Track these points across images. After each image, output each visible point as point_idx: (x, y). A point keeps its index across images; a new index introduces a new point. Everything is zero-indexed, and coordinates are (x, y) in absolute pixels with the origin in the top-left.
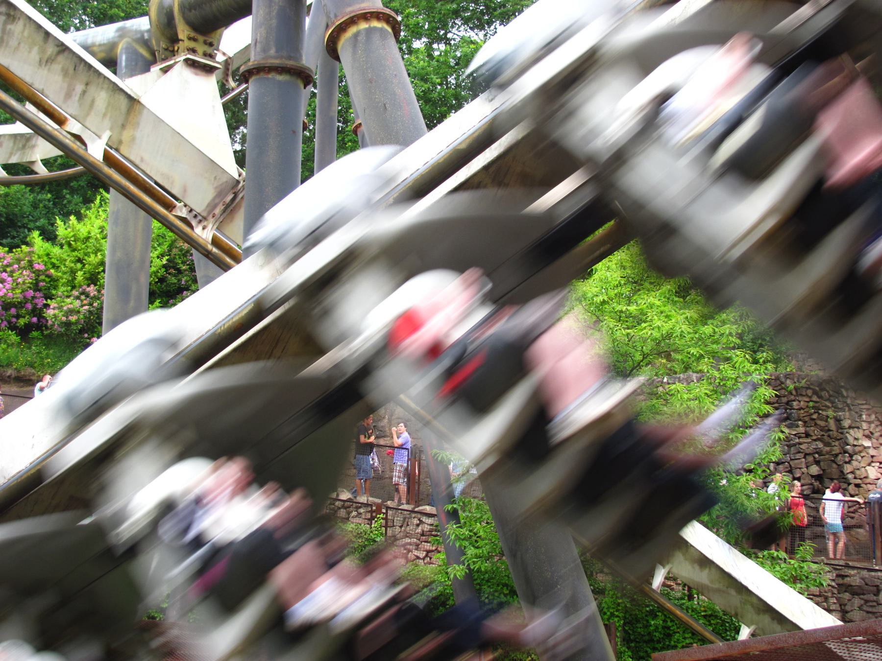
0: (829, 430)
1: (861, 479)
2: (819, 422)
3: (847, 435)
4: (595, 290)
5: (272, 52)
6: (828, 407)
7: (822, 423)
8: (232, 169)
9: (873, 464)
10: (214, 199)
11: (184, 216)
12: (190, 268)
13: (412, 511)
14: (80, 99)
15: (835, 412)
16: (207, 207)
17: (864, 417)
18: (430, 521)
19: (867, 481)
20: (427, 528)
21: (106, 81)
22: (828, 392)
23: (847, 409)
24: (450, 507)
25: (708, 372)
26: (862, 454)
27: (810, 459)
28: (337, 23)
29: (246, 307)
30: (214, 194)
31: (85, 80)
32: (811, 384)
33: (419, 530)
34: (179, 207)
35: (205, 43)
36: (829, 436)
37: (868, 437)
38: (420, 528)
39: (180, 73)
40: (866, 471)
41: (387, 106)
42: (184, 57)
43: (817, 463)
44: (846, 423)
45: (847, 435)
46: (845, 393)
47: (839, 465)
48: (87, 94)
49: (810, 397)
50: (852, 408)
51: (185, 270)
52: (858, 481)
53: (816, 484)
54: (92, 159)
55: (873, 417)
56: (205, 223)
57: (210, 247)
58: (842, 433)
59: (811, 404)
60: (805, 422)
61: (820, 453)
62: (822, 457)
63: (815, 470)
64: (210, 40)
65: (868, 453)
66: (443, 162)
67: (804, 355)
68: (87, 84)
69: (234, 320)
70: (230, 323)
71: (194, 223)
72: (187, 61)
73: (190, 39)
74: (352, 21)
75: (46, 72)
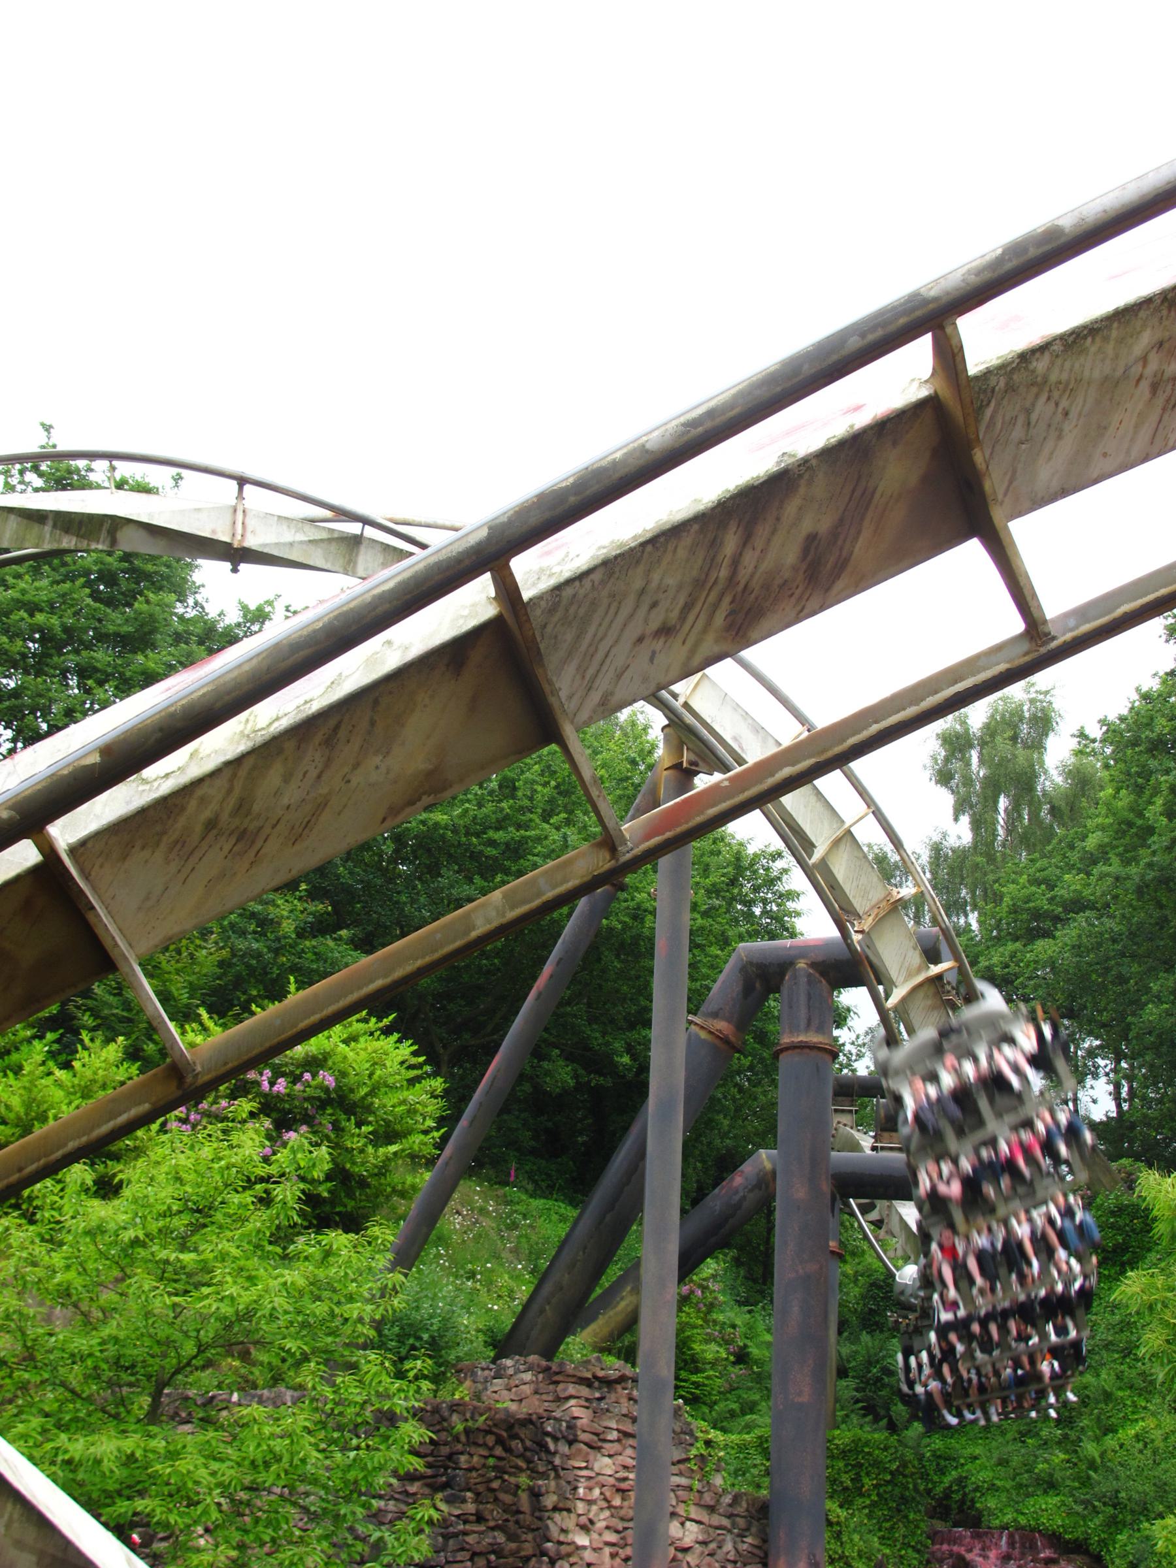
0: (519, 1512)
3: (549, 1522)
6: (521, 1470)
7: (507, 1498)
17: (581, 1491)
22: (522, 1441)
23: (552, 1474)
25: (314, 1388)
26: (572, 1560)
32: (495, 1425)
36: (517, 1522)
37: (584, 1529)
44: (550, 1501)
45: (549, 1522)
46: (552, 1446)
49: (491, 1449)
50: (562, 1473)
58: (540, 1519)
59: (491, 1461)
60: (478, 1494)
62: (502, 1560)
65: (581, 1559)
67: (487, 1372)
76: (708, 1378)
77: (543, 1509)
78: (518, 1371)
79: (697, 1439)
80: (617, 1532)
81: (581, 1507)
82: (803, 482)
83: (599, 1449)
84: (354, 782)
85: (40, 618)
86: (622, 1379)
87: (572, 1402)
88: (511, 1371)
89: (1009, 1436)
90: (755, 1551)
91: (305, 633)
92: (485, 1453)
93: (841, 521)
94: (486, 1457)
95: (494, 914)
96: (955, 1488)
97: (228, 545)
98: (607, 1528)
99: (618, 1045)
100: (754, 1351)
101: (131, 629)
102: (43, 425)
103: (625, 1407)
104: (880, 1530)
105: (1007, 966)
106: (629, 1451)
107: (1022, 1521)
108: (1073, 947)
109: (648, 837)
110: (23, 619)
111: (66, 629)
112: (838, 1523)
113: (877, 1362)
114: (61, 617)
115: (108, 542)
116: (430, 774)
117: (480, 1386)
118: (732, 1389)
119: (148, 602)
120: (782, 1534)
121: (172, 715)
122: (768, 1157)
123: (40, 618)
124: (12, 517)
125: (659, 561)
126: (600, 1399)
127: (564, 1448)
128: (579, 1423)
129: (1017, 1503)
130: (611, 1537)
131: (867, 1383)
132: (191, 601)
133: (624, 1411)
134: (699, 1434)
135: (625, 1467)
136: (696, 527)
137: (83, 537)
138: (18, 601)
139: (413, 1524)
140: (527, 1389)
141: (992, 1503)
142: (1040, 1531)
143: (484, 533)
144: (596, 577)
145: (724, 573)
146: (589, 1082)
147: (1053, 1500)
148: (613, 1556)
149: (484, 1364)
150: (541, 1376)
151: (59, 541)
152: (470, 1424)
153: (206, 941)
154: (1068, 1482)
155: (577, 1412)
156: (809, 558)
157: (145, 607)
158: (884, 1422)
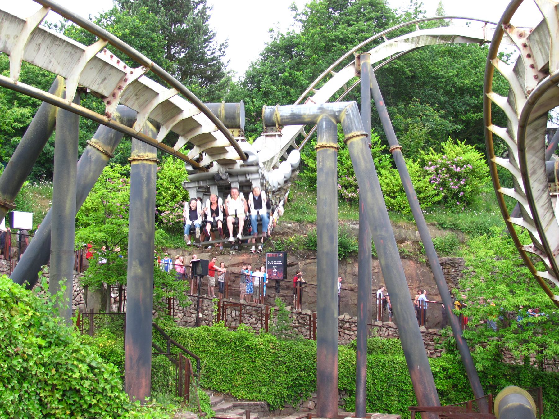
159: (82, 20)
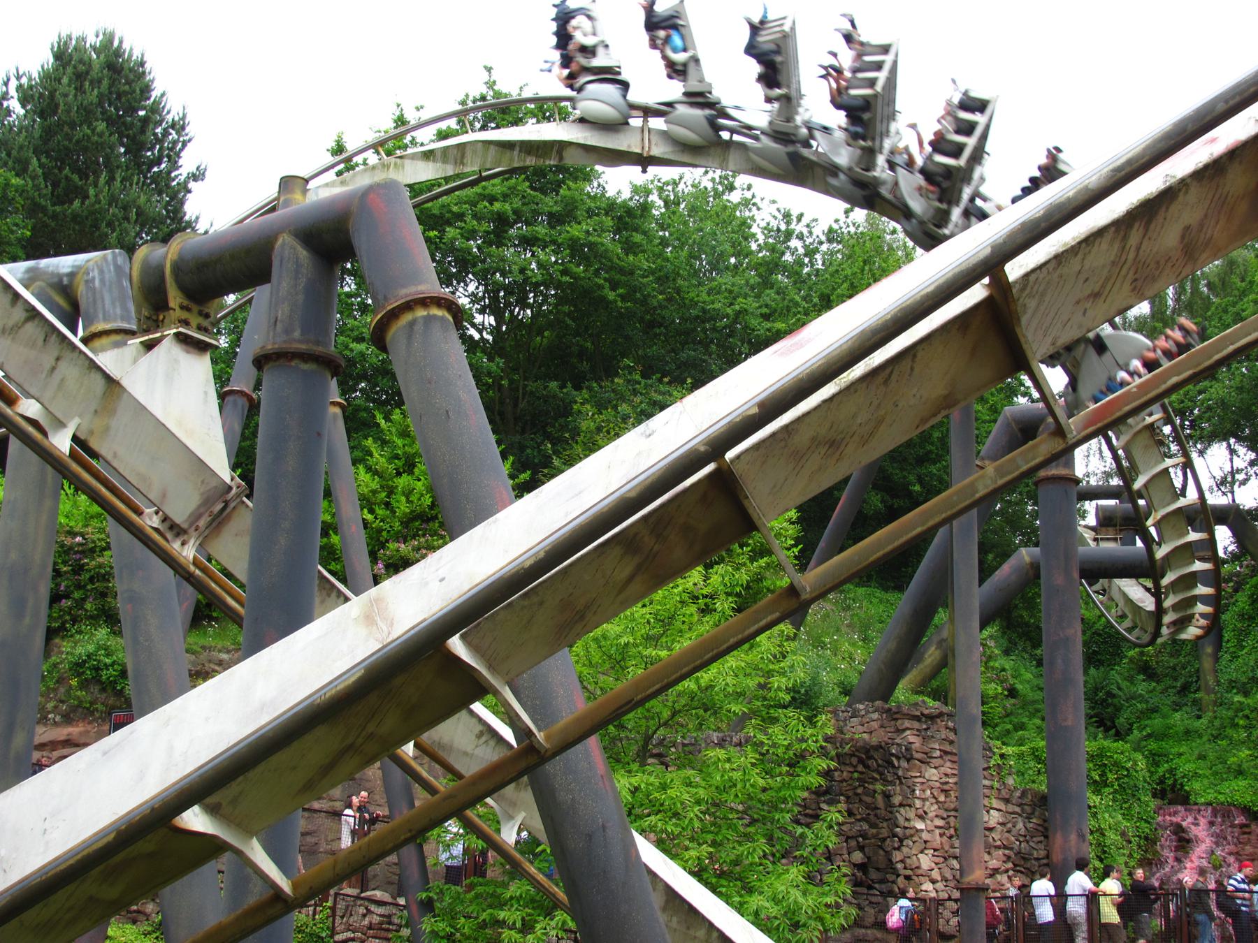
0: (878, 809)
1: (911, 869)
2: (866, 798)
3: (897, 814)
4: (618, 629)
5: (297, 334)
6: (876, 780)
7: (868, 799)
8: (224, 472)
9: (926, 852)
10: (199, 507)
11: (155, 525)
12: (72, 570)
13: (357, 897)
14: (47, 376)
15: (884, 785)
16: (189, 516)
17: (917, 792)
18: (381, 910)
19: (919, 872)
20: (376, 919)
21: (82, 356)
22: (876, 760)
23: (898, 782)
24: (424, 895)
25: (755, 737)
26: (915, 839)
27: (853, 843)
28: (389, 308)
29: (353, 675)
30: (199, 503)
31: (56, 354)
32: (857, 750)
33: (366, 922)
34: (148, 514)
35: (200, 313)
36: (876, 815)
37: (921, 818)
38: (367, 919)
39: (168, 349)
40: (918, 859)
41: (451, 413)
42: (175, 331)
43: (861, 848)
44: (897, 800)
45: (897, 814)
46: (896, 764)
47: (886, 852)
48: (56, 372)
49: (855, 767)
50: (904, 781)
51: (66, 572)
52: (908, 872)
53: (859, 874)
54: (58, 453)
55: (928, 792)
56: (185, 537)
57: (192, 568)
58: (891, 812)
59: (856, 775)
60: (848, 798)
61: (864, 836)
62: (867, 841)
63: (858, 857)
64: (207, 310)
65: (920, 838)
66: (607, 511)
67: (845, 714)
68: (58, 359)
69: (338, 688)
70: (333, 691)
71: (169, 536)
72: (177, 335)
73: (182, 307)
74: (408, 306)
75: (9, 342)
76: (991, 708)
77: (893, 806)
78: (868, 712)
79: (994, 753)
80: (943, 819)
81: (918, 803)
82: (1181, 194)
83: (928, 763)
84: (900, 405)
85: (497, 206)
86: (941, 715)
87: (908, 732)
88: (863, 713)
89: (1205, 739)
90: (1040, 828)
91: (880, 322)
92: (851, 770)
93: (1206, 216)
94: (852, 772)
95: (989, 482)
96: (1167, 776)
97: (640, 155)
98: (937, 816)
99: (912, 478)
100: (1019, 687)
101: (559, 209)
102: (485, 67)
103: (944, 734)
104: (1121, 809)
105: (1182, 402)
106: (948, 764)
107: (1222, 798)
108: (1237, 388)
109: (1086, 427)
110: (485, 207)
111: (515, 212)
112: (1095, 807)
113: (1102, 688)
114: (511, 204)
115: (557, 159)
116: (946, 397)
117: (841, 723)
118: (1008, 715)
119: (569, 189)
120: (1058, 817)
121: (801, 380)
122: (1028, 553)
123: (497, 206)
124: (492, 147)
125: (1090, 252)
126: (926, 729)
127: (904, 764)
128: (913, 746)
129: (1216, 785)
130: (940, 823)
131: (1096, 703)
132: (595, 184)
133: (943, 737)
134: (995, 750)
135: (946, 775)
136: (1113, 229)
137: (540, 157)
138: (480, 195)
139: (826, 824)
140: (875, 725)
141: (1197, 785)
142: (1235, 805)
143: (988, 250)
144: (1051, 266)
145: (1131, 256)
146: (893, 504)
147: (1242, 783)
148: (941, 835)
149: (843, 708)
150: (884, 715)
151: (525, 161)
152: (840, 750)
153: (625, 423)
154: (1252, 770)
155: (911, 739)
156: (1186, 241)
157: (567, 193)
158: (1113, 732)
159: (963, 267)
